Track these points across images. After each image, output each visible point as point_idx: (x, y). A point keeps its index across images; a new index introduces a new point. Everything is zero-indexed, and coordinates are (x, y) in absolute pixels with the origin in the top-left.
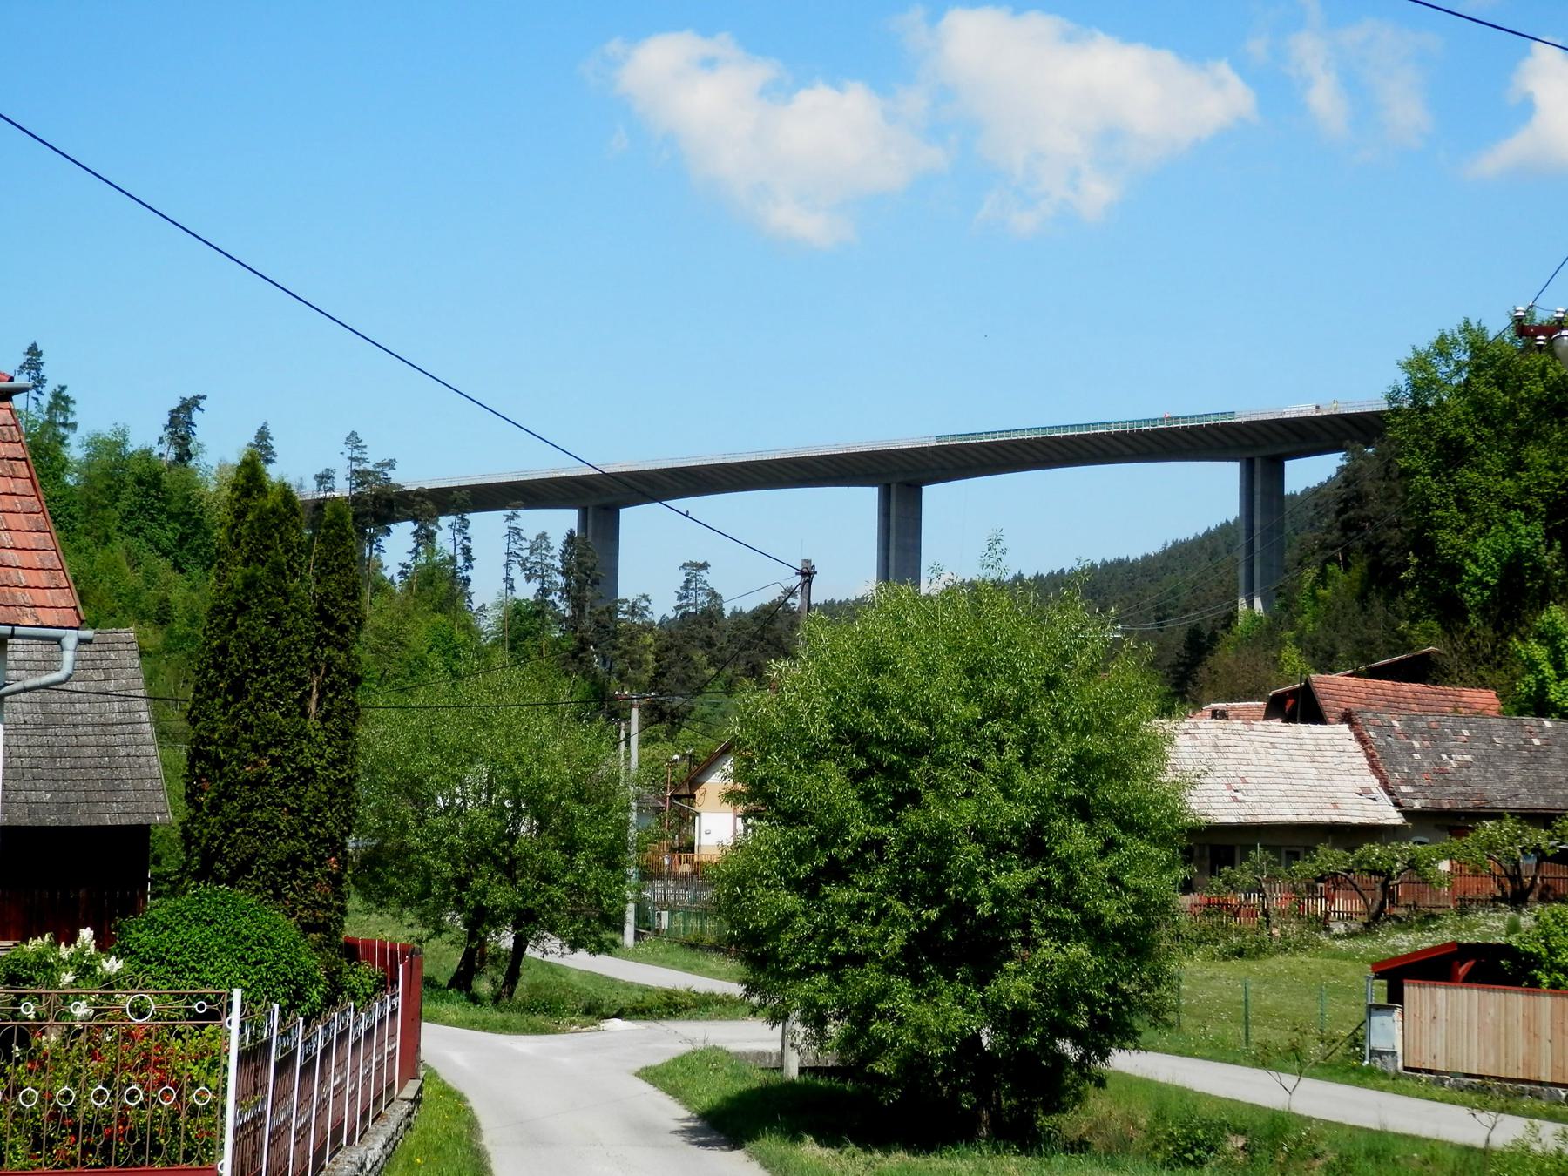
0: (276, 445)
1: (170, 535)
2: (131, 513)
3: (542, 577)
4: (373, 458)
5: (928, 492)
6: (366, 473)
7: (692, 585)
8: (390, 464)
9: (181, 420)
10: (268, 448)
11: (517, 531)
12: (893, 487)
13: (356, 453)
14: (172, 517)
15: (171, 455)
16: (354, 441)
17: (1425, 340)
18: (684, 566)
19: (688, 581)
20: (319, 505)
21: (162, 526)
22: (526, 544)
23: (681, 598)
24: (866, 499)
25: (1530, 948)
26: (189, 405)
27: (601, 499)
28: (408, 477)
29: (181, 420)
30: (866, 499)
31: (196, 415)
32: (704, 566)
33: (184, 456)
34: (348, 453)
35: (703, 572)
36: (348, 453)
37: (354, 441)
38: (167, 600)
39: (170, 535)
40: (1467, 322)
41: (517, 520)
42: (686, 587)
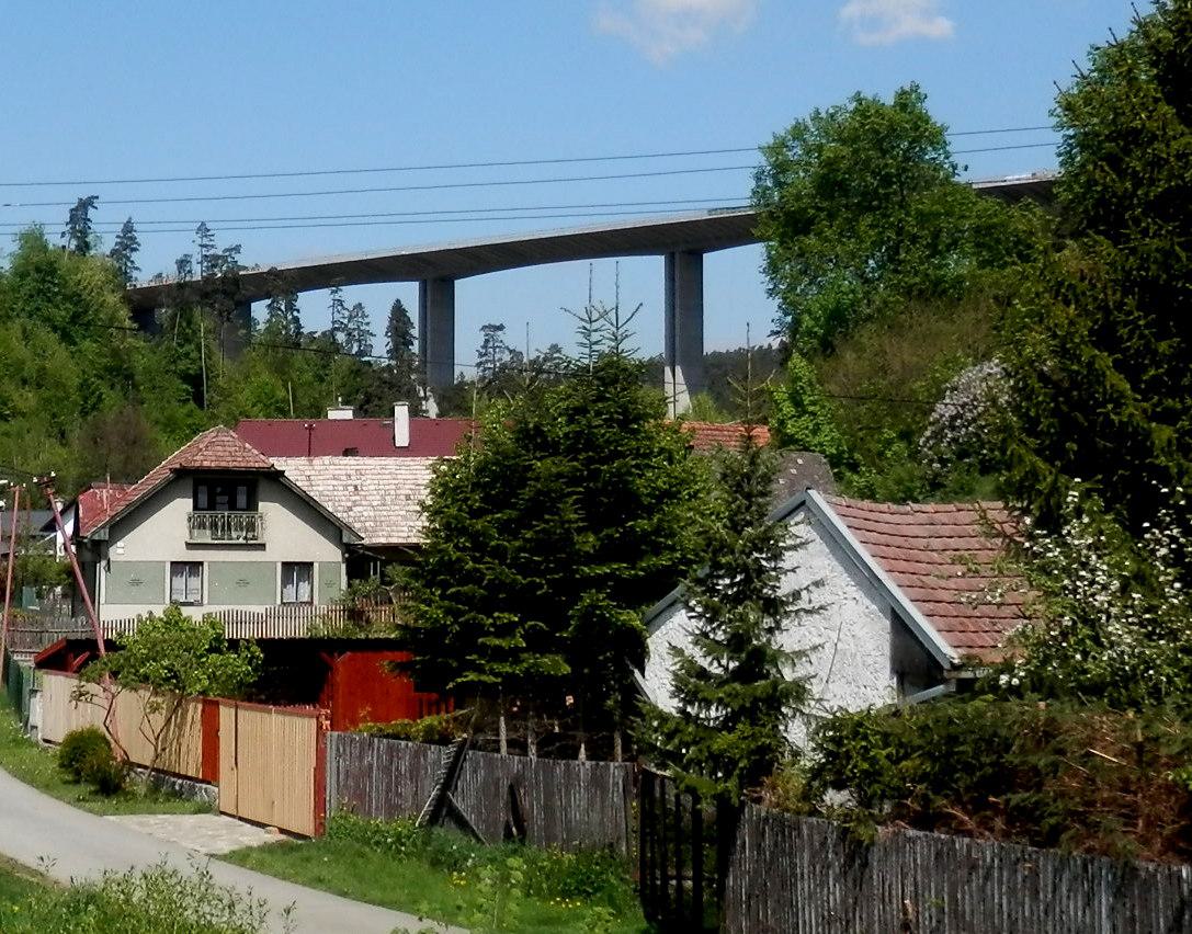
0: (140, 237)
1: (63, 313)
2: (31, 296)
3: (359, 341)
4: (220, 245)
5: (710, 259)
6: (217, 257)
7: (491, 344)
8: (237, 249)
9: (80, 215)
10: (133, 239)
11: (341, 302)
12: (677, 256)
13: (205, 241)
14: (67, 298)
15: (73, 244)
16: (203, 230)
17: (783, 126)
18: (484, 328)
19: (487, 341)
20: (181, 286)
21: (57, 307)
22: (347, 314)
23: (481, 355)
24: (650, 270)
25: (339, 515)
26: (86, 204)
27: (438, 273)
28: (257, 257)
29: (80, 215)
30: (650, 270)
31: (91, 213)
32: (500, 328)
33: (84, 247)
34: (199, 241)
35: (500, 333)
36: (199, 241)
37: (203, 230)
38: (45, 369)
39: (63, 313)
40: (818, 112)
41: (340, 293)
42: (485, 347)
